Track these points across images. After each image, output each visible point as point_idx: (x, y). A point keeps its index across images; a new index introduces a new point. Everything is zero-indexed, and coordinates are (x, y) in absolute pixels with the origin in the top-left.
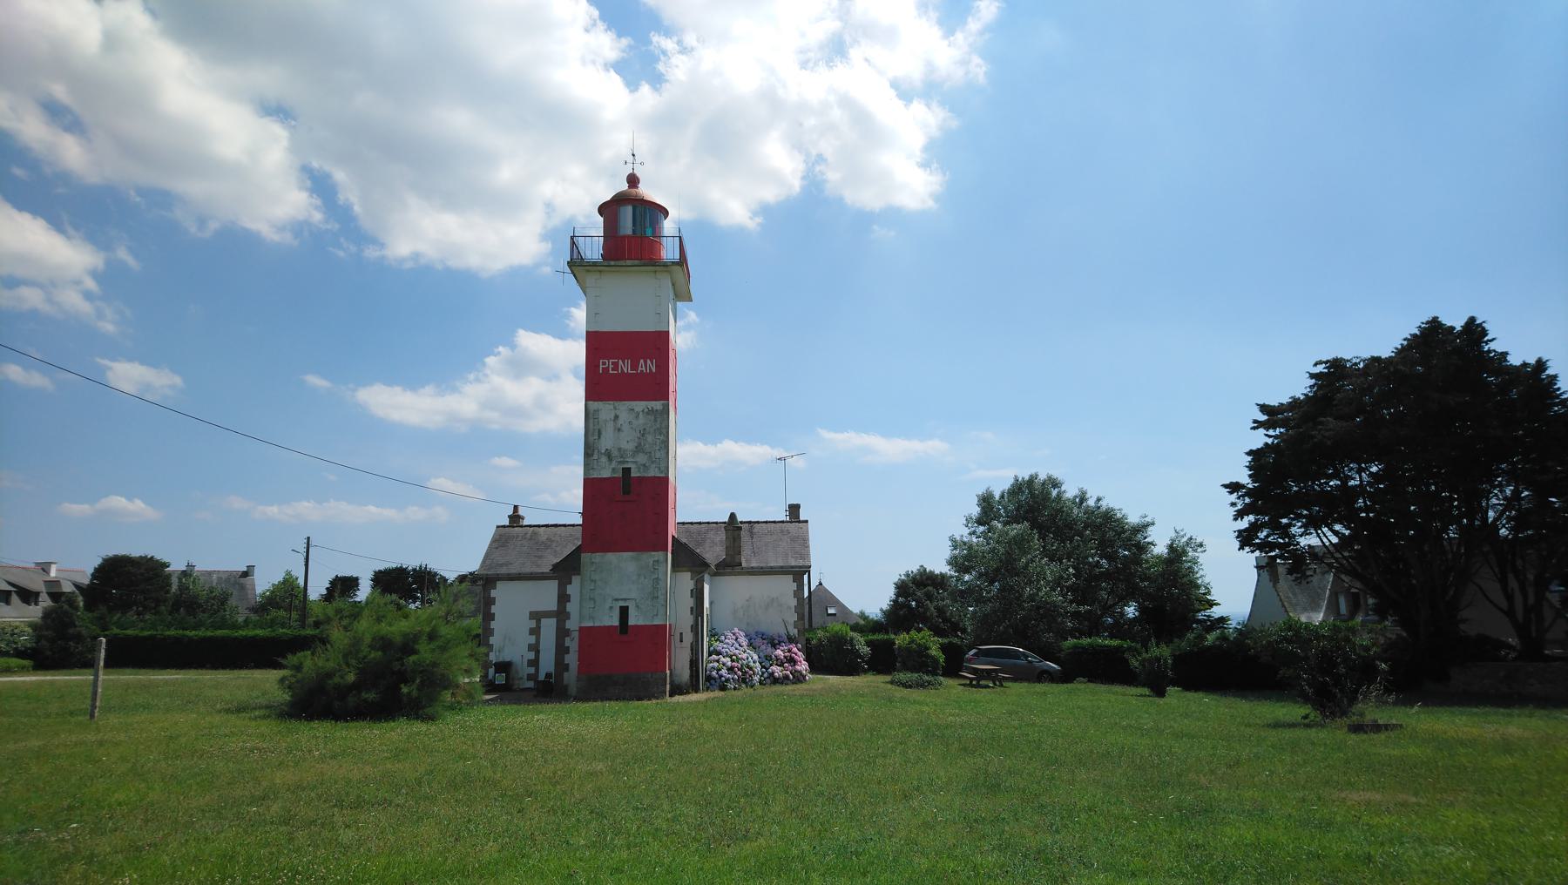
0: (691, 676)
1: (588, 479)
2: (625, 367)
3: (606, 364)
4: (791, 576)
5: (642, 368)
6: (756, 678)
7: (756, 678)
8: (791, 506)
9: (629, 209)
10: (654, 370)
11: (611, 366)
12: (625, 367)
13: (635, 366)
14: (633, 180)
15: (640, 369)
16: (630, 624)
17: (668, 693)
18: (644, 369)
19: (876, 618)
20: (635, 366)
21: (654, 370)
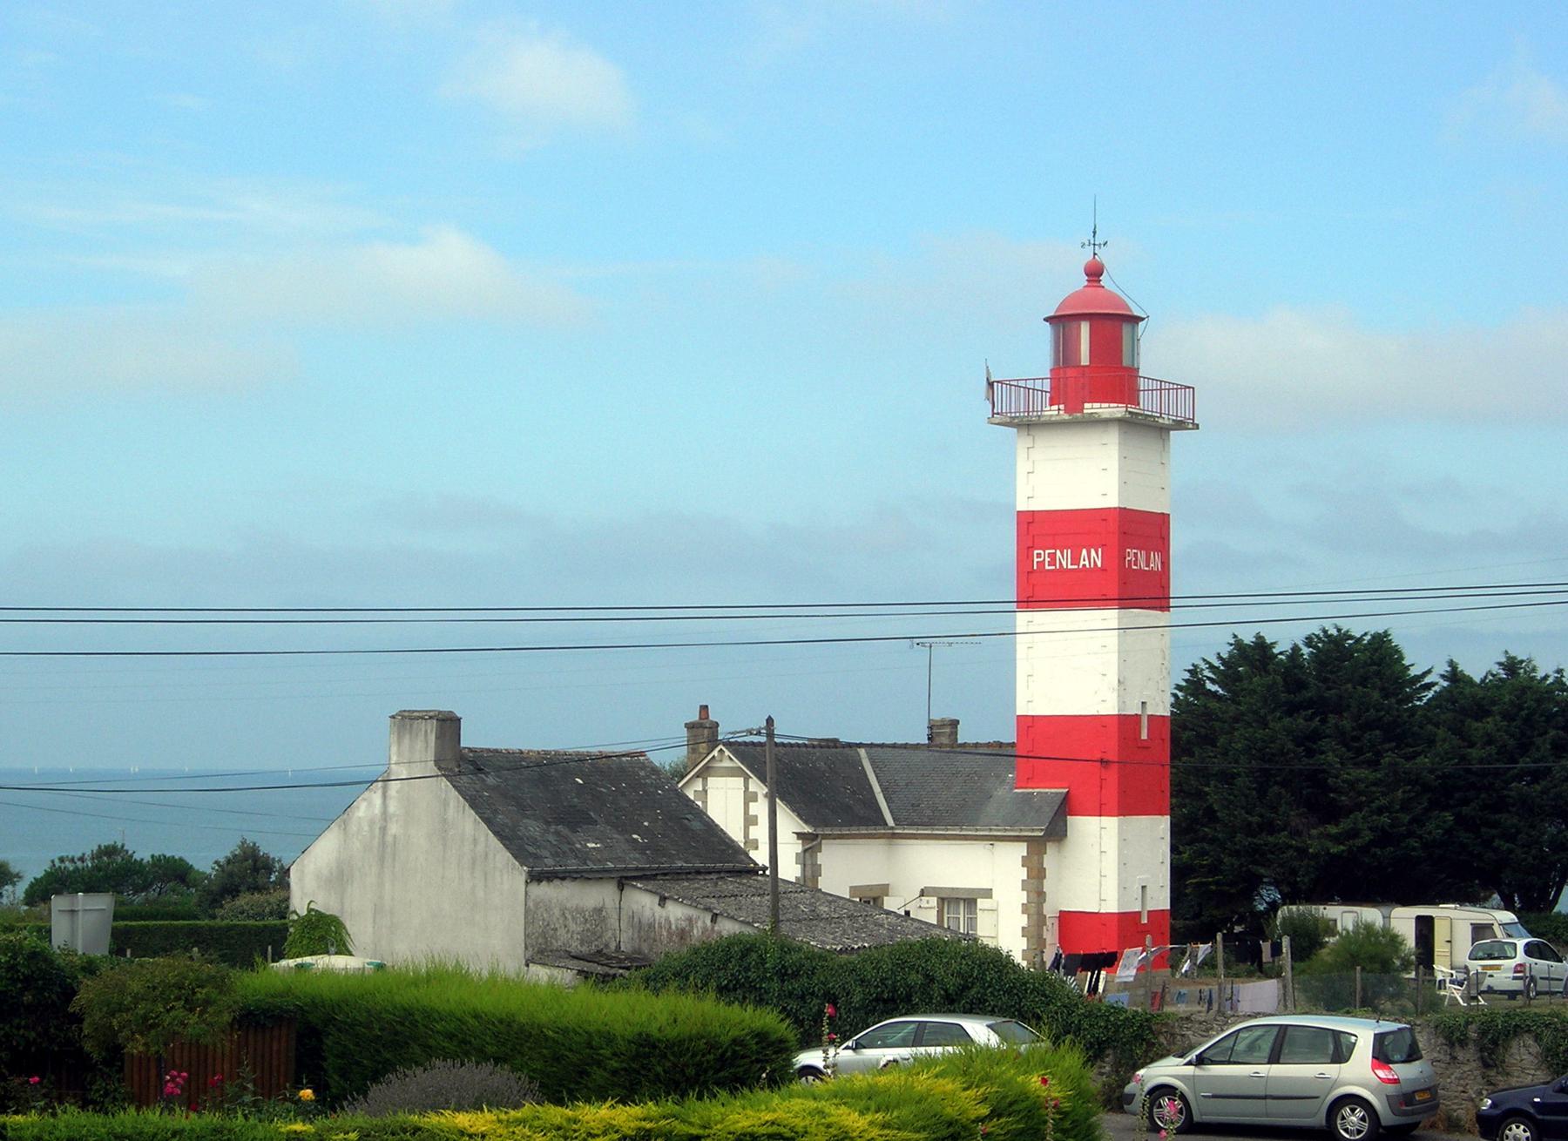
0: (748, 784)
1: (1123, 793)
2: (1064, 560)
3: (1041, 556)
4: (751, 827)
5: (1084, 562)
6: (1260, 734)
7: (1260, 734)
8: (1143, 703)
9: (1085, 328)
10: (1099, 564)
11: (1047, 559)
12: (1064, 560)
13: (1076, 559)
14: (1094, 273)
15: (1082, 563)
16: (1169, 817)
17: (1358, 1005)
18: (1087, 563)
19: (658, 765)
20: (1076, 559)
21: (1099, 564)
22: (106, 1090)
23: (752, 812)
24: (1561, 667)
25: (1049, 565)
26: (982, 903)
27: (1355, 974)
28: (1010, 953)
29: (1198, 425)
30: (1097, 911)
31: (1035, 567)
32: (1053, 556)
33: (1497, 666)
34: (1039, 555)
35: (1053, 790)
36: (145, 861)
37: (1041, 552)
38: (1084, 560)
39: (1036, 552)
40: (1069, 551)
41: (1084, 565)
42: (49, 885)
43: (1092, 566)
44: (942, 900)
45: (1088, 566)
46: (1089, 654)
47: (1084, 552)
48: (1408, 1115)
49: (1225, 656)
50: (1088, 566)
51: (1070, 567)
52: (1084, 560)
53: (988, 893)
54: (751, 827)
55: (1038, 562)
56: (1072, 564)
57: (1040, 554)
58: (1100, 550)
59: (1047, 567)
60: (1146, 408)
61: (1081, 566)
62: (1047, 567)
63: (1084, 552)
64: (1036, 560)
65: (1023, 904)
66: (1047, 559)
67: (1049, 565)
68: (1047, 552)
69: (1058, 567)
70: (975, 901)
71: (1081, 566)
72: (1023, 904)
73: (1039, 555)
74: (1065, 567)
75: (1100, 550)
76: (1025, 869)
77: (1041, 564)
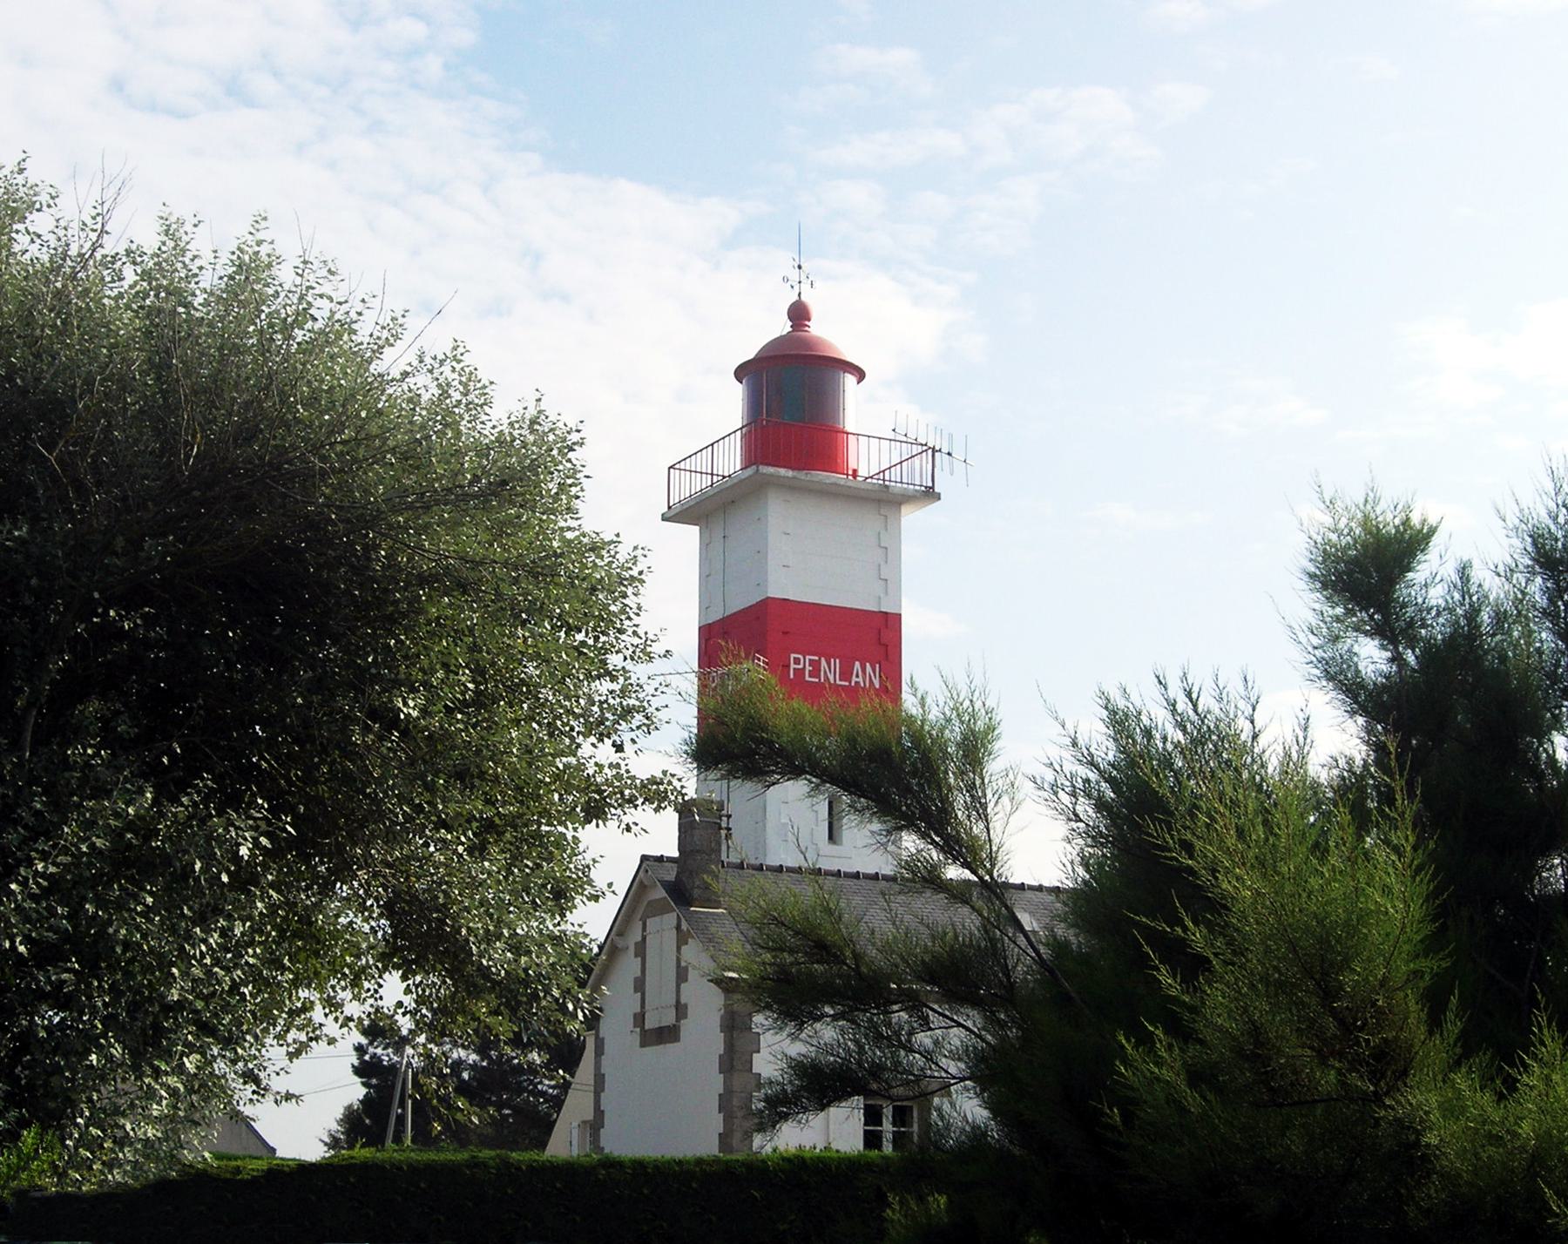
15: (854, 679)
18: (860, 679)
22: (1429, 1112)
24: (332, 1046)
25: (810, 676)
28: (1501, 569)
29: (667, 651)
32: (816, 666)
33: (1450, 572)
34: (797, 661)
36: (1359, 762)
37: (800, 656)
38: (857, 676)
39: (793, 656)
40: (837, 661)
41: (857, 683)
42: (516, 1169)
49: (387, 973)
51: (838, 682)
52: (857, 676)
55: (794, 669)
56: (840, 680)
57: (799, 659)
59: (807, 678)
60: (893, 479)
61: (853, 684)
62: (807, 678)
64: (793, 666)
66: (808, 668)
67: (810, 676)
68: (808, 657)
71: (853, 684)
74: (832, 682)
77: (801, 671)
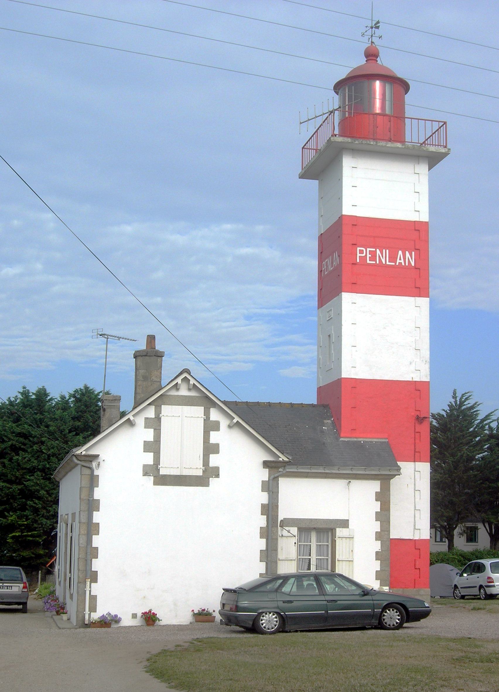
4: (212, 433)
10: (413, 264)
11: (368, 256)
15: (398, 261)
18: (402, 261)
20: (393, 258)
23: (151, 431)
26: (340, 532)
27: (26, 532)
30: (412, 539)
31: (358, 261)
34: (361, 252)
35: (375, 440)
38: (400, 259)
39: (358, 249)
40: (387, 251)
41: (400, 263)
43: (407, 264)
44: (300, 530)
45: (403, 264)
46: (352, 355)
47: (400, 253)
48: (379, 618)
50: (403, 264)
51: (388, 263)
52: (400, 259)
53: (345, 524)
54: (212, 433)
58: (413, 253)
59: (368, 262)
61: (397, 264)
62: (368, 262)
63: (400, 253)
65: (376, 532)
68: (368, 250)
69: (378, 262)
70: (333, 531)
71: (397, 264)
72: (376, 532)
73: (361, 252)
74: (384, 263)
75: (413, 253)
76: (379, 503)
